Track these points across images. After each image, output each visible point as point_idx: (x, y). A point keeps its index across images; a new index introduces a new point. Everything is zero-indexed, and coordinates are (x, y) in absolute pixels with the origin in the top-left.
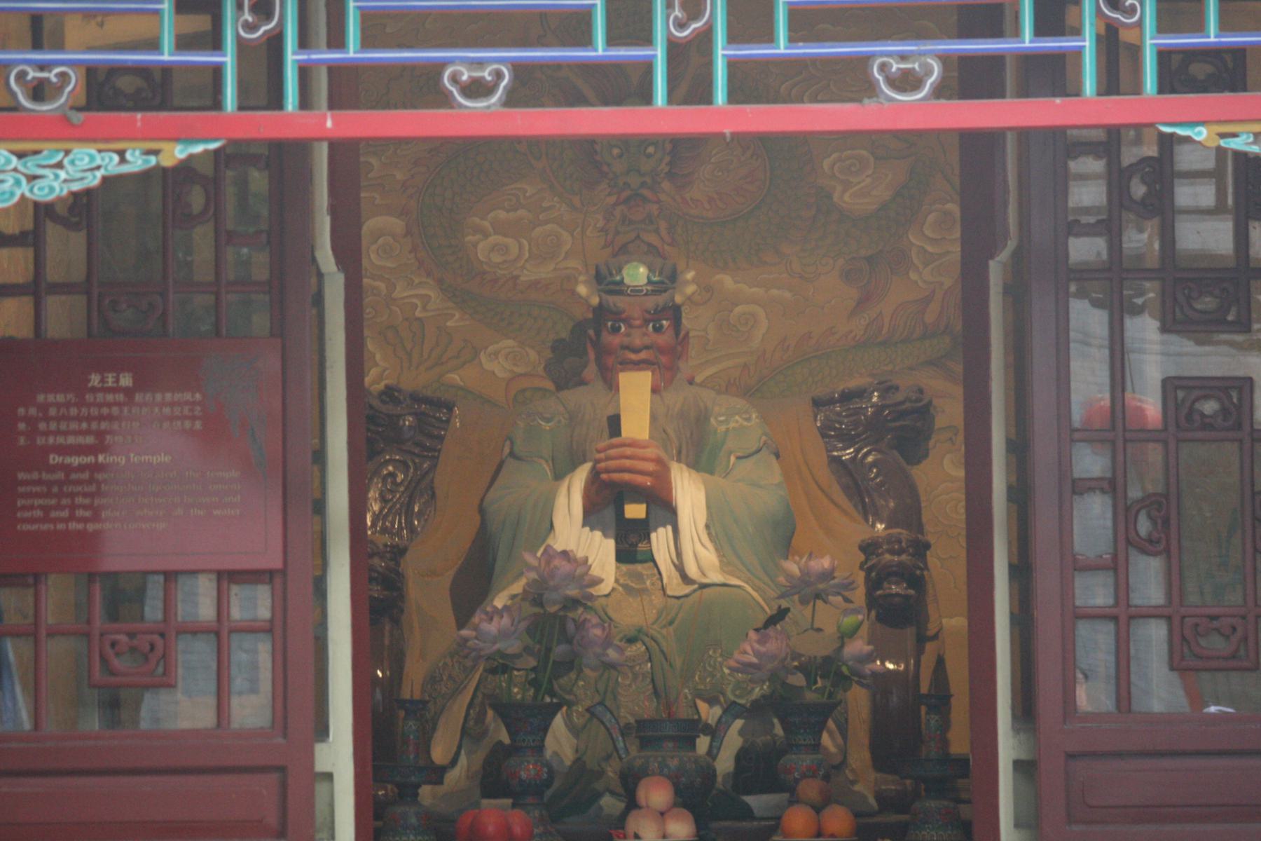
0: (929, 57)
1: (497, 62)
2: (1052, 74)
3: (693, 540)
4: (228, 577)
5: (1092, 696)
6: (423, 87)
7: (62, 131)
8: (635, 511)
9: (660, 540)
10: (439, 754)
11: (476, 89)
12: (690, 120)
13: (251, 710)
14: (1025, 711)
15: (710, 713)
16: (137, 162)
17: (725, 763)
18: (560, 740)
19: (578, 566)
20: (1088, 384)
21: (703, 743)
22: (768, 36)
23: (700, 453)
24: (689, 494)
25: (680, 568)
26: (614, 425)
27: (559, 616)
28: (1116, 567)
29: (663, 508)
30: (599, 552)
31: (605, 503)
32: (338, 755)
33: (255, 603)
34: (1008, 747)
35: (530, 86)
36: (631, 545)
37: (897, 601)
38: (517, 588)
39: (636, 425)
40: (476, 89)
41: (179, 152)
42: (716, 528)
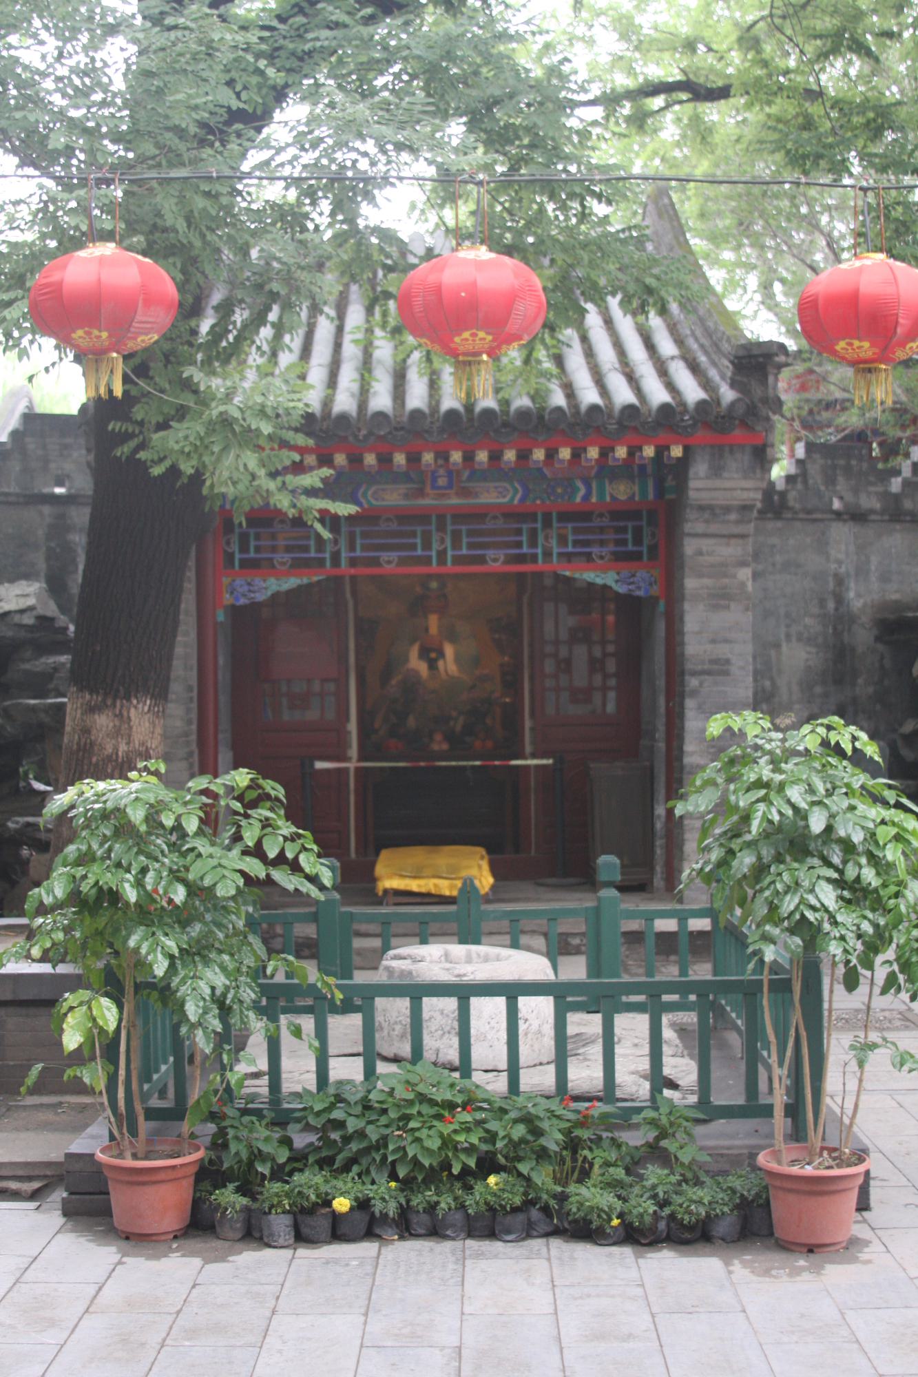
0: (501, 554)
1: (394, 555)
2: (534, 558)
3: (449, 663)
4: (324, 681)
5: (550, 710)
6: (375, 562)
7: (288, 574)
8: (433, 655)
9: (441, 664)
10: (377, 725)
11: (389, 562)
12: (442, 570)
13: (330, 715)
14: (532, 715)
15: (454, 714)
16: (305, 581)
17: (458, 728)
18: (411, 722)
19: (416, 672)
20: (549, 627)
21: (452, 723)
22: (461, 549)
23: (452, 637)
24: (449, 650)
25: (446, 671)
26: (427, 630)
27: (411, 685)
28: (605, 655)
29: (441, 654)
30: (422, 668)
31: (424, 653)
32: (353, 726)
33: (331, 687)
34: (528, 724)
35: (402, 561)
36: (432, 665)
37: (511, 681)
38: (400, 677)
39: (434, 629)
40: (389, 562)
41: (315, 579)
42: (458, 660)
